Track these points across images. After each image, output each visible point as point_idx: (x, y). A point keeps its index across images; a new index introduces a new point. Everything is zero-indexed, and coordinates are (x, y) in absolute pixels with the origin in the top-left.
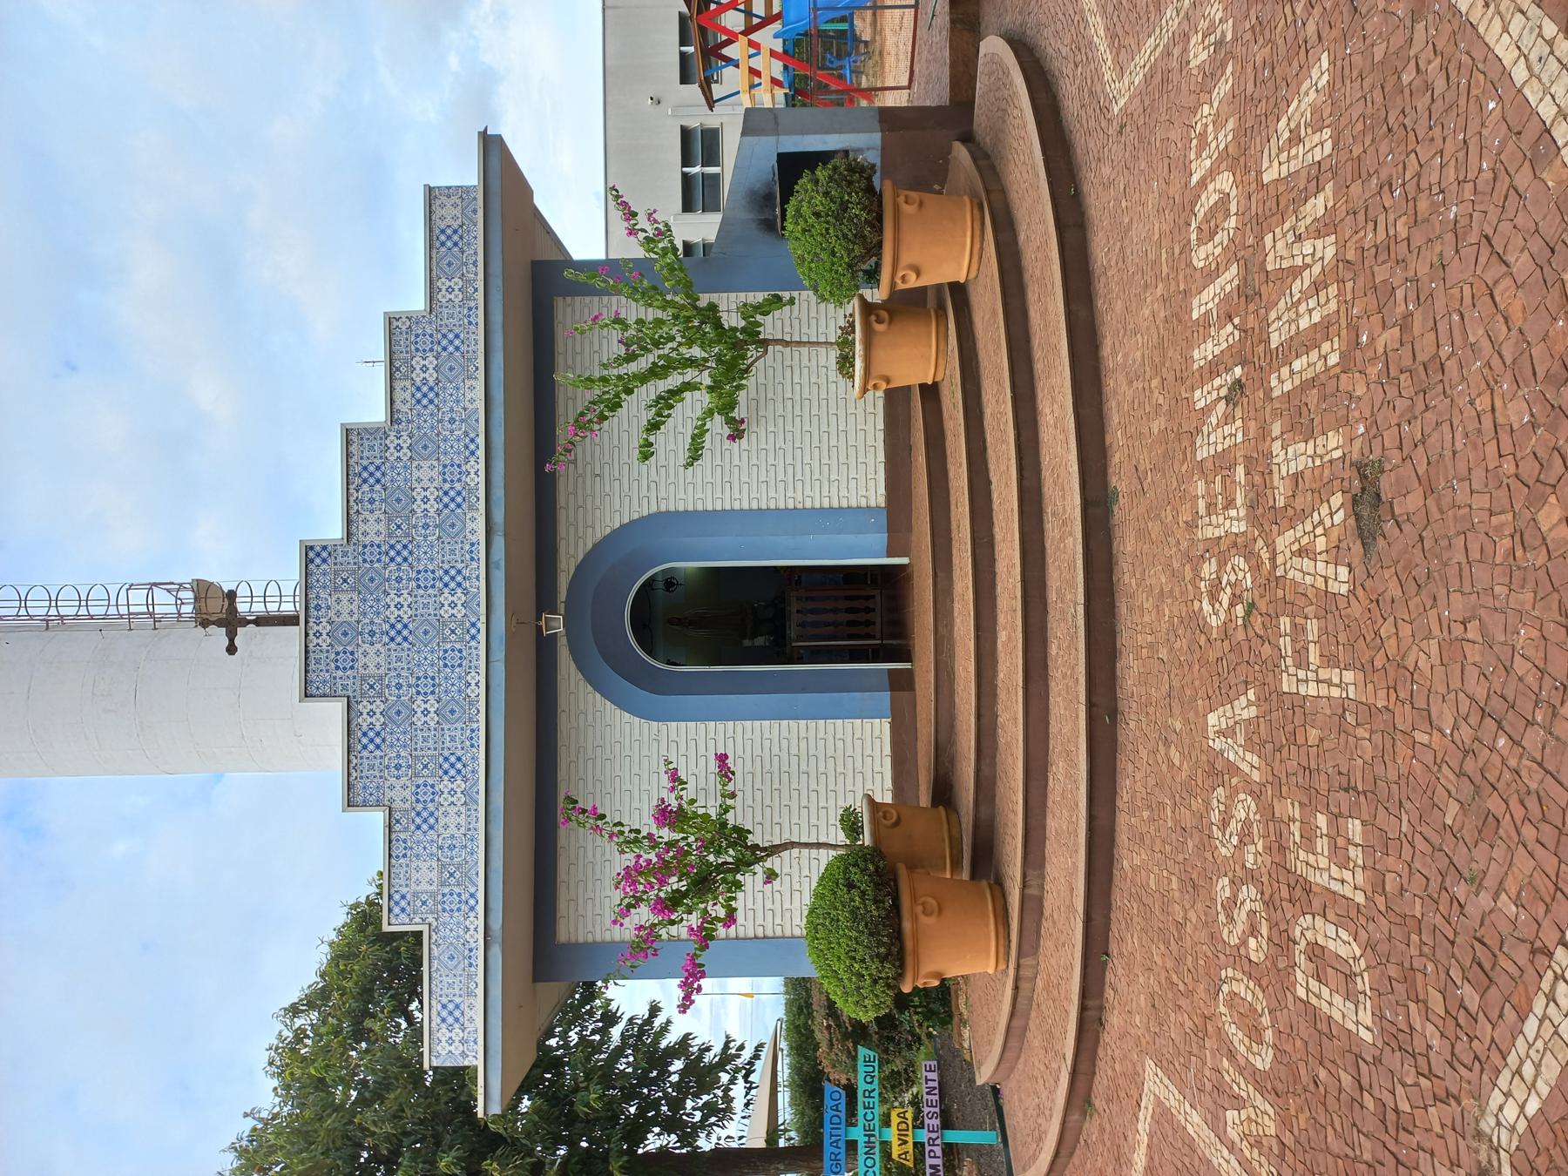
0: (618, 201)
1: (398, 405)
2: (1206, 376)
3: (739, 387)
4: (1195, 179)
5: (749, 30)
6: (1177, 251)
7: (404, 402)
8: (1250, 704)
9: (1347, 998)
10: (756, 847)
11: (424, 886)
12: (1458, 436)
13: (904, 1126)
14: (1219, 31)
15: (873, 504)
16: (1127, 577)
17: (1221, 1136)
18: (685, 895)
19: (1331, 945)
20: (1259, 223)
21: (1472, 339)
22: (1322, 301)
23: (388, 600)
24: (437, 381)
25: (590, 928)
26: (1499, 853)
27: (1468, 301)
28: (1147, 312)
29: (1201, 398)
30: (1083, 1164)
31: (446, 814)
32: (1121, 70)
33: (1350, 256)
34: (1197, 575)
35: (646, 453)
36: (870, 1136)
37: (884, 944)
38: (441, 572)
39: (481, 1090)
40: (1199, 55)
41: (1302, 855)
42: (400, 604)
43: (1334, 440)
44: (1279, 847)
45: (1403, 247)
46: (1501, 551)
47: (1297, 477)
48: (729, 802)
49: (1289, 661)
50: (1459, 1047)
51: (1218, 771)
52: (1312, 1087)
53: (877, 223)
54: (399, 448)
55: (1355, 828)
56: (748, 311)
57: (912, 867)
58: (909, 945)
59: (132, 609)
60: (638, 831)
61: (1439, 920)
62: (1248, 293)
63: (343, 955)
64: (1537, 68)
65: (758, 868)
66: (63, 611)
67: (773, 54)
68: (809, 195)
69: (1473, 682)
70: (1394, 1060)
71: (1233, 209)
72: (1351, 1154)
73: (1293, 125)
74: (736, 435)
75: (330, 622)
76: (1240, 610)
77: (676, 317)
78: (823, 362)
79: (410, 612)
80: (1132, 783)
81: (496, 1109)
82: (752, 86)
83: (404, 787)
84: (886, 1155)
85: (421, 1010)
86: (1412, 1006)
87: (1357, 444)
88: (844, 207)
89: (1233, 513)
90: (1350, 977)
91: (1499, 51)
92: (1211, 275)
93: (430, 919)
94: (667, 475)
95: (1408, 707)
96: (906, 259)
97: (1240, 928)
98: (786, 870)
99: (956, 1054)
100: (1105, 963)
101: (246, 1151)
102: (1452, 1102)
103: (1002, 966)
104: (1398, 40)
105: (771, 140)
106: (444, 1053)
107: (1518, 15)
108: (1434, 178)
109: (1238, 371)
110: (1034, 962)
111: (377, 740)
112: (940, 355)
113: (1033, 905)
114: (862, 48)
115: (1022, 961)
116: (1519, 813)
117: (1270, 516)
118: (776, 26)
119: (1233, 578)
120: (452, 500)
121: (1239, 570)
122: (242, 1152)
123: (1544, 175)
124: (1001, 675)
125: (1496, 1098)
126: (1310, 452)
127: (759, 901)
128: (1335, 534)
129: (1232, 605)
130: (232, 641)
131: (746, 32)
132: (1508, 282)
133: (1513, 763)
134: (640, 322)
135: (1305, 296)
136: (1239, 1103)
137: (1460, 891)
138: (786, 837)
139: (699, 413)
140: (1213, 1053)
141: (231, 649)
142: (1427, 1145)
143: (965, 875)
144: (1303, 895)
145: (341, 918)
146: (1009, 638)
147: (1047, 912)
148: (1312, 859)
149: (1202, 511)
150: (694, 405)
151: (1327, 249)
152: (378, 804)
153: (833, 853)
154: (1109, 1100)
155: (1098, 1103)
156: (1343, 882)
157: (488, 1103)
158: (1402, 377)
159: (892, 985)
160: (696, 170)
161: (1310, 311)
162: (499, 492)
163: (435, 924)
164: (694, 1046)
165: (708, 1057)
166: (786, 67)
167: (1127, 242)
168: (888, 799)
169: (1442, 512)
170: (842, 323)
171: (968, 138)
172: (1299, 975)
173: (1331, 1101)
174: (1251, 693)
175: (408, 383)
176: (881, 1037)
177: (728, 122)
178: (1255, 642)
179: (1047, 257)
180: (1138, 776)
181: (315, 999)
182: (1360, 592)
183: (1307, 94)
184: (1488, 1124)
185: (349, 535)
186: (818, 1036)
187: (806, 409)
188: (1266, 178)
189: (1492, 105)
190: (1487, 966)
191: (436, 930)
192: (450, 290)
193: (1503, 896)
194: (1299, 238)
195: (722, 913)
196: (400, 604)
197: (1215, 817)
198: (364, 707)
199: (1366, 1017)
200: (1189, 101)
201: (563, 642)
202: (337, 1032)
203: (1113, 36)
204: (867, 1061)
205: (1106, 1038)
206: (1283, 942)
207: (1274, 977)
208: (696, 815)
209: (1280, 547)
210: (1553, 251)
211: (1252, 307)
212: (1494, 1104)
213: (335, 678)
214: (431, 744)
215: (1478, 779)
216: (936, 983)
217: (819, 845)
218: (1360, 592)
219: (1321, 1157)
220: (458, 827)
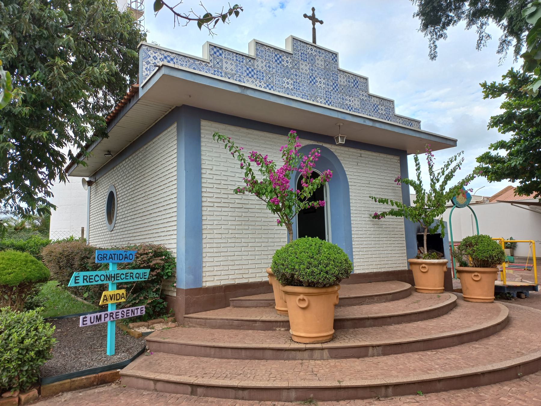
1: (373, 98)
13: (118, 297)
23: (322, 79)
25: (207, 136)
36: (114, 277)
38: (330, 101)
79: (319, 86)
93: (211, 64)
106: (149, 53)
110: (325, 357)
111: (278, 61)
112: (436, 291)
115: (326, 351)
163: (209, 65)
175: (378, 103)
185: (340, 70)
213: (298, 51)
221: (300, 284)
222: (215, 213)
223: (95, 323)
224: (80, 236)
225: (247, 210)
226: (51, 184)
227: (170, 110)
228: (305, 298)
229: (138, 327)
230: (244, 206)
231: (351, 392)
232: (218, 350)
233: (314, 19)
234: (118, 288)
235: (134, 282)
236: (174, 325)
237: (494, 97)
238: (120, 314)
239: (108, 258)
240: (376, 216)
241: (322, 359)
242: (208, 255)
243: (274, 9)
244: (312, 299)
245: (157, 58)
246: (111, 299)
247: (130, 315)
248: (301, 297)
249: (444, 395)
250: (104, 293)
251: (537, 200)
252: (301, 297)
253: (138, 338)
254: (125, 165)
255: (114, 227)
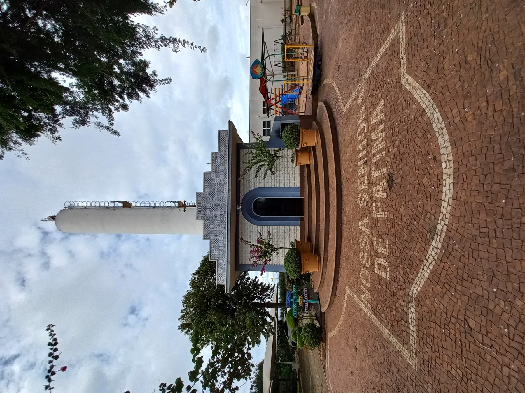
0: (252, 133)
1: (213, 169)
2: (360, 160)
3: (273, 165)
4: (358, 124)
5: (276, 103)
6: (355, 138)
7: (214, 168)
8: (367, 220)
9: (385, 272)
10: (275, 248)
11: (216, 253)
12: (408, 167)
14: (363, 97)
15: (297, 187)
16: (345, 198)
17: (360, 299)
18: (262, 256)
19: (382, 263)
20: (370, 131)
21: (411, 149)
22: (382, 144)
24: (220, 164)
26: (414, 243)
27: (410, 142)
28: (349, 149)
29: (359, 164)
30: (334, 307)
31: (220, 241)
32: (344, 105)
33: (388, 136)
34: (358, 197)
35: (256, 177)
37: (298, 265)
39: (226, 289)
40: (359, 101)
41: (377, 247)
42: (212, 204)
43: (384, 170)
44: (372, 246)
45: (398, 134)
46: (416, 187)
47: (377, 177)
48: (270, 240)
49: (375, 211)
50: (406, 279)
51: (361, 232)
52: (378, 289)
53: (299, 135)
54: (213, 176)
55: (387, 241)
56: (275, 151)
57: (304, 252)
58: (303, 266)
59: (168, 206)
60: (254, 244)
61: (403, 257)
62: (368, 144)
63: (203, 265)
64: (422, 99)
65: (275, 252)
66: (156, 206)
67: (280, 107)
68: (286, 130)
69: (410, 212)
70: (393, 283)
71: (365, 129)
72: (385, 301)
73: (377, 113)
74: (273, 174)
75: (201, 206)
76: (366, 203)
77: (262, 152)
78: (288, 160)
80: (344, 236)
81: (228, 292)
82: (276, 113)
83: (213, 236)
84: (298, 305)
85: (215, 275)
86: (397, 273)
87: (389, 170)
88: (293, 132)
89: (365, 185)
90: (385, 269)
91: (415, 96)
92: (361, 141)
93: (217, 259)
94: (260, 181)
95: (397, 218)
96: (304, 141)
97: (365, 261)
98: (280, 253)
99: (311, 287)
100: (339, 269)
101: (186, 297)
102: (404, 290)
103: (320, 270)
104: (396, 96)
105: (280, 121)
107: (419, 90)
108: (403, 120)
109: (366, 159)
113: (326, 259)
114: (296, 107)
116: (418, 235)
117: (372, 185)
118: (281, 103)
119: (364, 197)
120: (222, 185)
121: (366, 195)
122: (185, 298)
123: (424, 118)
124: (321, 217)
125: (412, 288)
126: (379, 172)
127: (275, 258)
128: (384, 187)
129: (364, 202)
130: (185, 209)
131: (275, 104)
132: (417, 138)
133: (417, 227)
134: (255, 153)
135: (379, 144)
136: (364, 293)
137: (407, 251)
138: (280, 247)
139: (266, 170)
140: (359, 285)
141: (185, 211)
142: (399, 298)
143: (313, 254)
144: (377, 254)
145: (202, 259)
146: (322, 210)
147: (328, 260)
148: (378, 247)
149: (359, 185)
150: (265, 167)
151: (383, 135)
152: (209, 238)
153: (289, 250)
154: (339, 294)
155: (337, 295)
156: (384, 251)
157: (227, 291)
158: (397, 157)
159: (300, 273)
160: (266, 129)
161: (380, 146)
162: (230, 183)
164: (263, 285)
165: (266, 286)
166: (282, 110)
167: (345, 137)
168: (299, 240)
169: (405, 181)
170: (292, 153)
171: (316, 120)
172: (376, 269)
173: (381, 292)
174: (367, 218)
175: (215, 165)
176: (297, 283)
177: (272, 120)
178: (369, 208)
179: (330, 140)
180: (346, 235)
181: (197, 273)
182: (389, 197)
183: (379, 107)
184: (410, 293)
185: (204, 191)
186: (285, 283)
187: (285, 169)
188: (372, 123)
189: (414, 106)
190: (411, 264)
191: (218, 261)
192: (222, 148)
193: (415, 251)
194: (378, 133)
195: (269, 259)
196: (212, 204)
197: (360, 241)
198: (206, 221)
199: (388, 276)
200: (357, 110)
201: (240, 210)
202: (201, 278)
203: (343, 100)
204: (295, 287)
205: (339, 283)
206: (373, 263)
207: (371, 270)
208: (264, 242)
209: (373, 190)
210: (425, 131)
211: (369, 147)
212: (412, 290)
214: (217, 228)
215: (411, 230)
216: (307, 273)
217: (286, 248)
218: (389, 197)
219: (379, 302)
220: (222, 243)
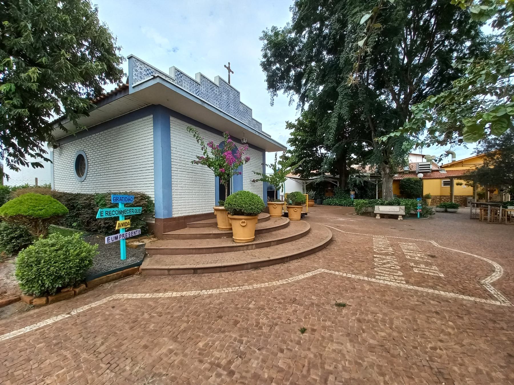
221: (242, 214)
222: (179, 175)
223: (114, 241)
224: (35, 184)
225: (195, 174)
226: (42, 145)
227: (147, 106)
228: (245, 221)
229: (132, 242)
230: (194, 172)
231: (274, 262)
232: (197, 250)
233: (230, 70)
234: (126, 219)
235: (131, 215)
236: (155, 239)
237: (289, 129)
238: (128, 234)
239: (119, 200)
240: (254, 181)
241: (252, 249)
242: (175, 199)
243: (169, 51)
244: (248, 222)
245: (140, 68)
246: (123, 226)
247: (133, 235)
248: (243, 221)
249: (306, 258)
250: (118, 222)
251: (299, 177)
252: (243, 221)
253: (135, 248)
254: (95, 137)
255: (85, 179)
